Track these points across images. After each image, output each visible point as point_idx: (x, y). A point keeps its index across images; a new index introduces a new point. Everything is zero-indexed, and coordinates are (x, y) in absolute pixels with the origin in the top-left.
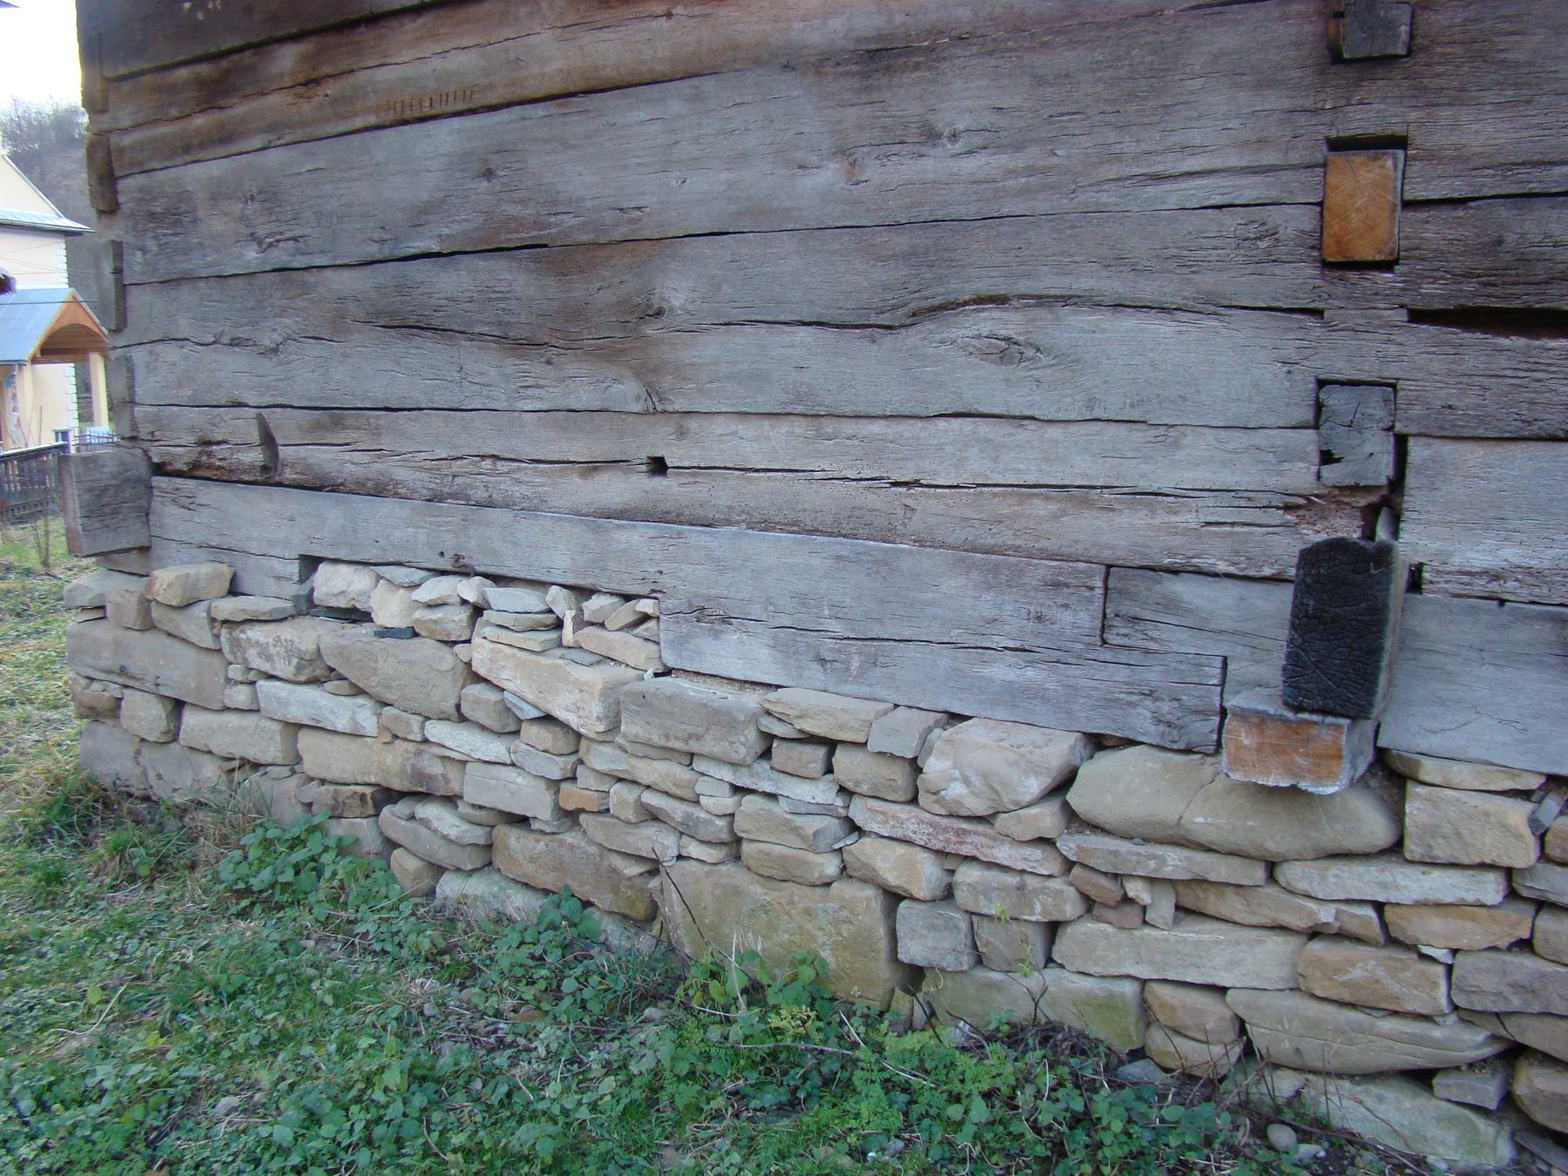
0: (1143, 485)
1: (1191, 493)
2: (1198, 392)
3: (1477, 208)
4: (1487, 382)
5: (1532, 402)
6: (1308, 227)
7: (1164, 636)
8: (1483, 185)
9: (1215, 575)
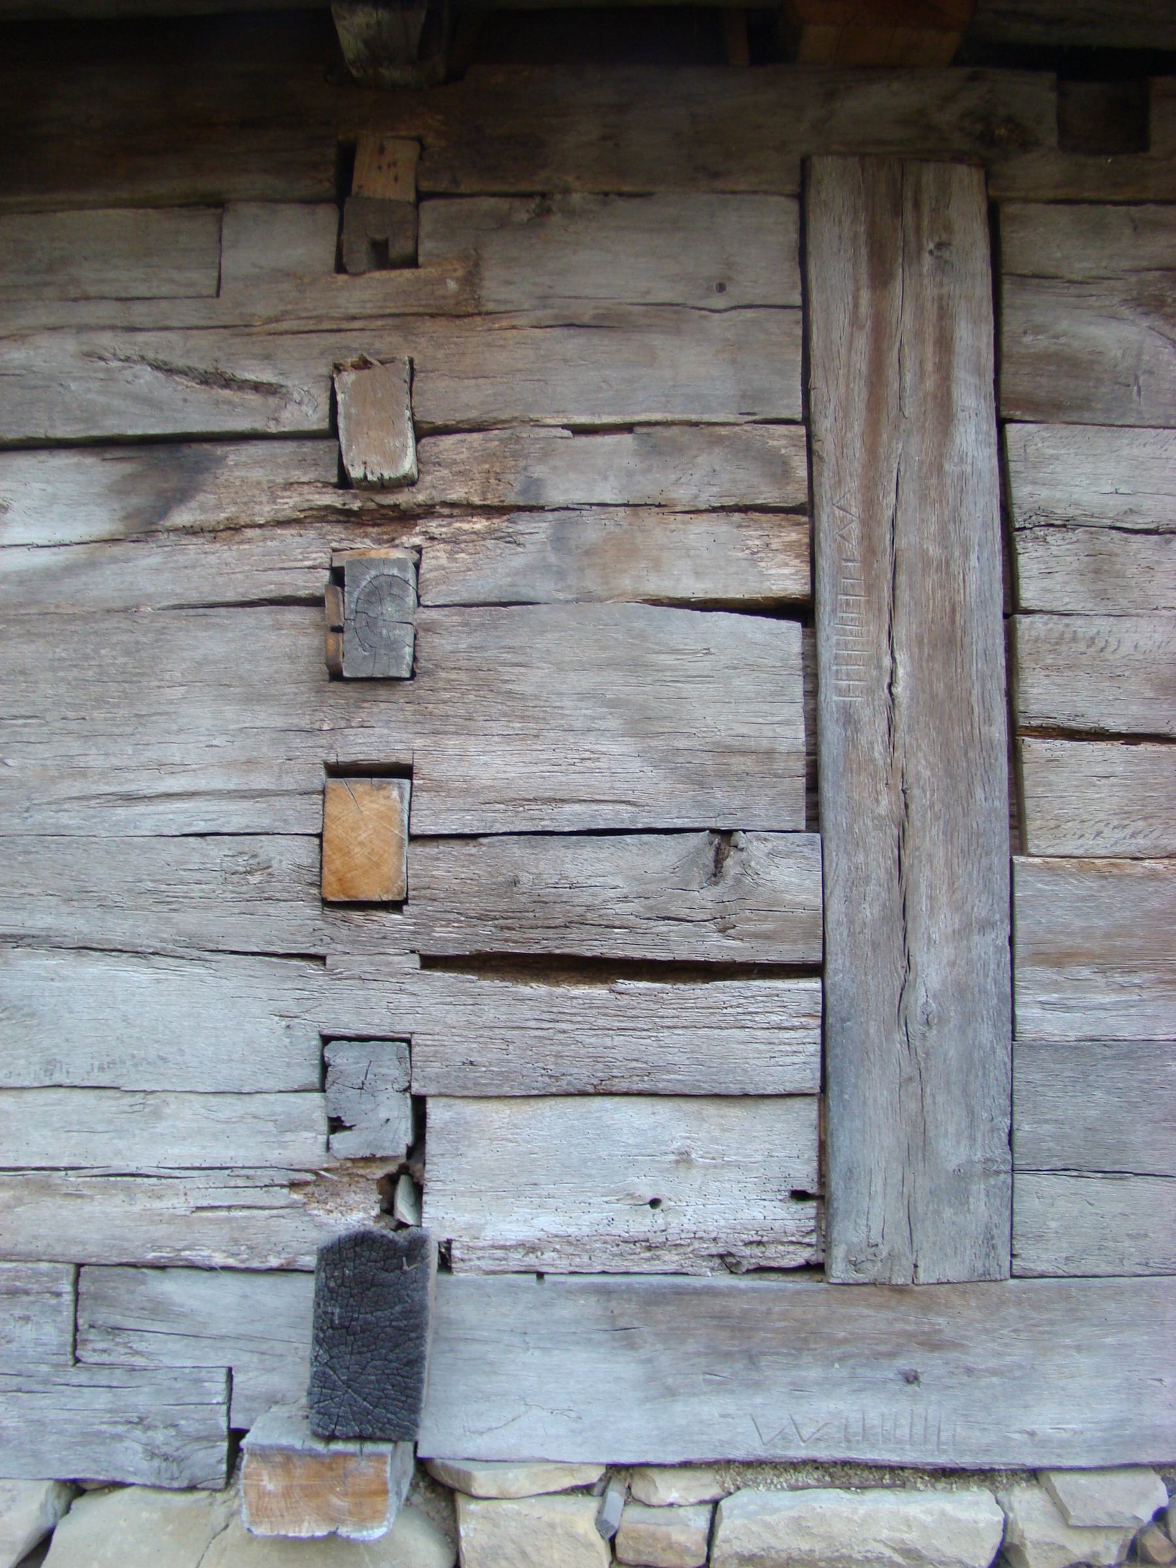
0: (119, 1165)
1: (176, 1173)
2: (181, 1052)
3: (490, 845)
4: (509, 1034)
5: (558, 1056)
6: (307, 861)
7: (153, 1348)
8: (495, 821)
9: (211, 1269)
